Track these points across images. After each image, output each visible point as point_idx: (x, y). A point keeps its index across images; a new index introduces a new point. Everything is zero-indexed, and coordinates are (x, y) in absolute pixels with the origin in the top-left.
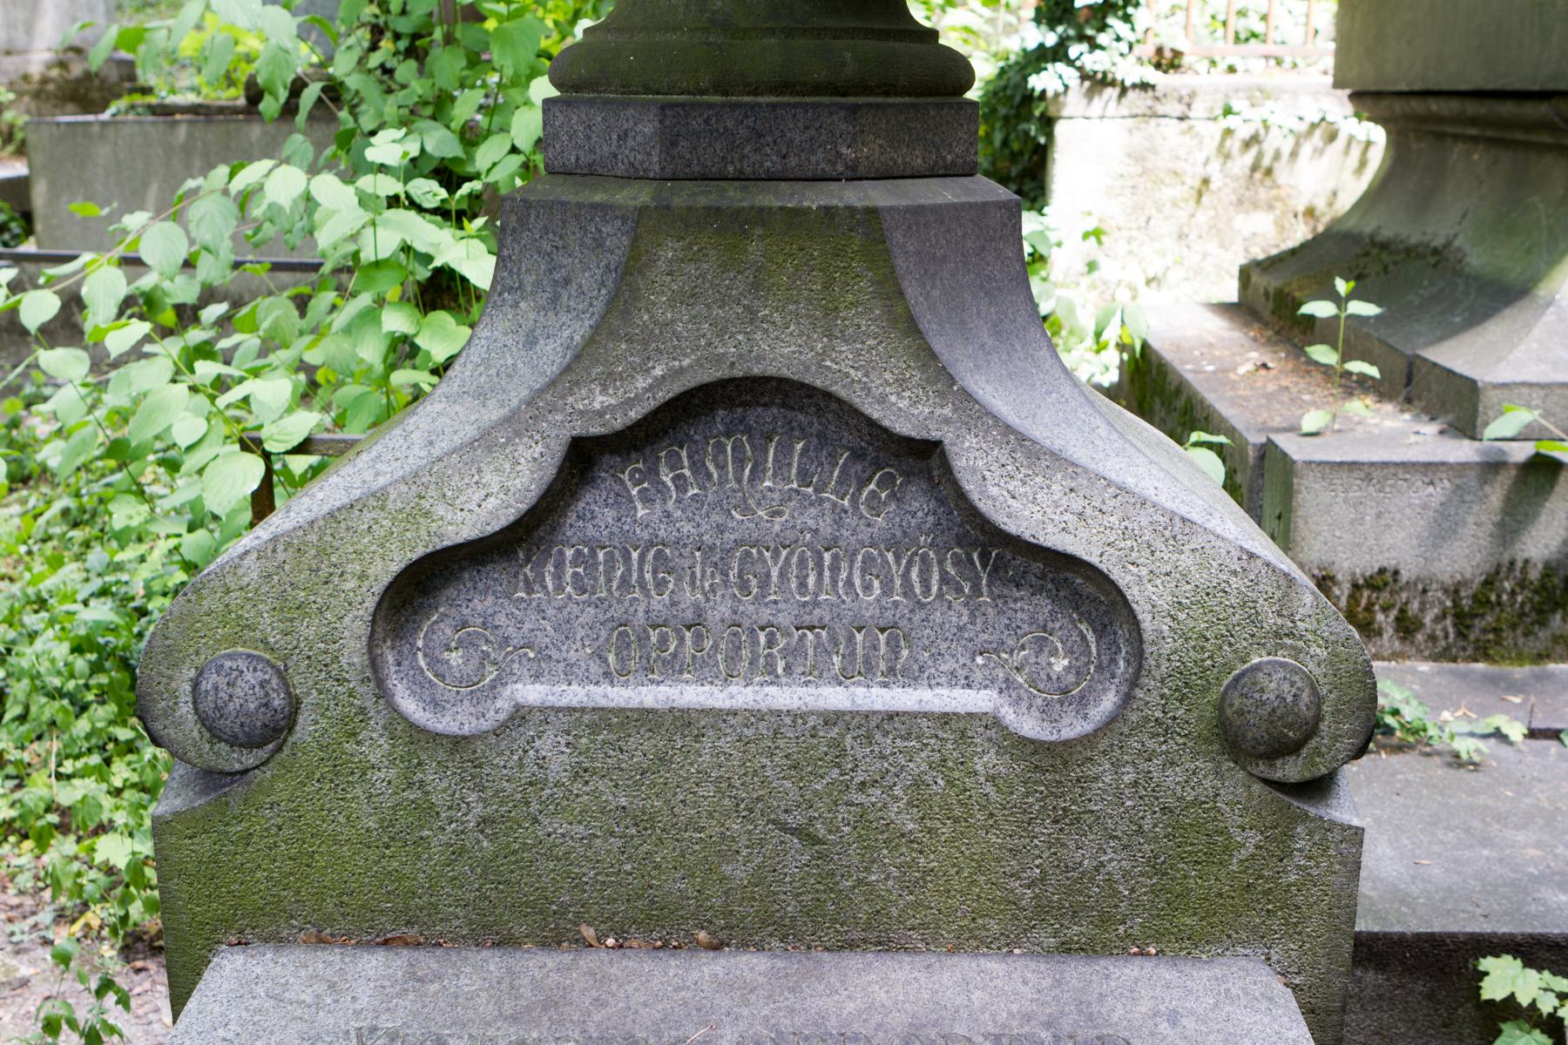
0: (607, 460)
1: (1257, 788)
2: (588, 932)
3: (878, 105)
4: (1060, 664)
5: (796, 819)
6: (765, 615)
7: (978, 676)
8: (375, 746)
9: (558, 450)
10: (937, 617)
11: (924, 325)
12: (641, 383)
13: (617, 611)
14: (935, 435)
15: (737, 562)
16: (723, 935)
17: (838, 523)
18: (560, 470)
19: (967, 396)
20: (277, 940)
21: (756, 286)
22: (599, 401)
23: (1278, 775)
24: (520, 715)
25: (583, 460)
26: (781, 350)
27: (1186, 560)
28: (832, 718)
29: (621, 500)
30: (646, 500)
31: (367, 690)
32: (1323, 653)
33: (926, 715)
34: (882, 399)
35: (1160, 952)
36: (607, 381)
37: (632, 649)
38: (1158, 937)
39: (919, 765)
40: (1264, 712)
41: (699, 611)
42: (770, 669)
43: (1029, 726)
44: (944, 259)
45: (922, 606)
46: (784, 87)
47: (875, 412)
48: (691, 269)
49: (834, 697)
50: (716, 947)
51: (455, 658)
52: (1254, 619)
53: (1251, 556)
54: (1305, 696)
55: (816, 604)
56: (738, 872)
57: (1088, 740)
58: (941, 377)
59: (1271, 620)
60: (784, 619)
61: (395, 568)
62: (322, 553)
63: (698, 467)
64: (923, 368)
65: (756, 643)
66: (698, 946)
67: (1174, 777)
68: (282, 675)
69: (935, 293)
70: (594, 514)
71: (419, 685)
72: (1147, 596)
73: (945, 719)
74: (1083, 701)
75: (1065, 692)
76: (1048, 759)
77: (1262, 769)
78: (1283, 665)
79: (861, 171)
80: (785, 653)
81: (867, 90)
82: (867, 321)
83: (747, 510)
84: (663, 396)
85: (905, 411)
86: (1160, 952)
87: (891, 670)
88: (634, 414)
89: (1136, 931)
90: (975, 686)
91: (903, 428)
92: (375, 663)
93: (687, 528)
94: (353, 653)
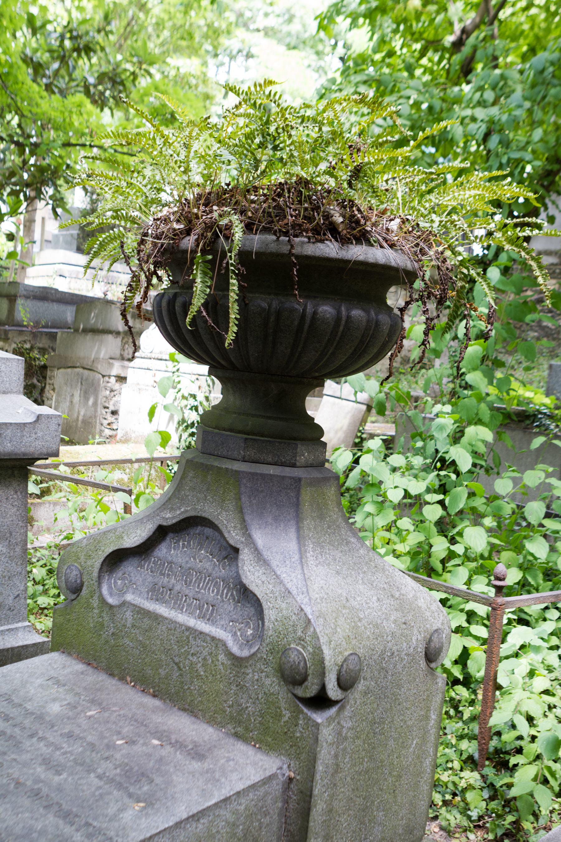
0: (171, 535)
1: (290, 695)
2: (129, 679)
3: (254, 440)
4: (250, 632)
5: (177, 660)
6: (187, 592)
7: (229, 628)
8: (95, 602)
9: (155, 527)
10: (226, 606)
11: (245, 510)
12: (178, 512)
13: (156, 580)
14: (238, 546)
15: (186, 574)
16: (157, 693)
17: (213, 569)
18: (154, 533)
19: (250, 536)
20: (69, 654)
21: (208, 489)
22: (168, 515)
23: (295, 692)
24: (124, 604)
25: (161, 533)
26: (208, 510)
27: (284, 605)
28: (188, 629)
29: (169, 549)
30: (174, 549)
31: (96, 584)
32: (311, 650)
33: (209, 635)
34: (229, 532)
35: (259, 748)
36: (172, 509)
37: (157, 593)
38: (261, 742)
39: (205, 653)
40: (289, 665)
41: (173, 585)
42: (182, 610)
43: (235, 650)
44: (262, 491)
45: (223, 601)
46: (231, 430)
47: (226, 535)
48: (195, 480)
49: (192, 622)
50: (154, 696)
51: (119, 582)
52: (295, 632)
53: (302, 610)
54: (302, 664)
55: (199, 592)
56: (162, 672)
57: (247, 659)
58: (245, 528)
59: (299, 633)
60: (191, 595)
61: (111, 551)
62: (99, 542)
63: (189, 542)
64: (241, 524)
65: (181, 600)
66: (149, 694)
67: (268, 682)
68: (81, 574)
69: (254, 502)
70: (163, 551)
71: (110, 588)
72: (270, 614)
73: (213, 638)
74: (251, 646)
75: (248, 642)
76: (238, 662)
77: (291, 687)
78: (298, 650)
79: (246, 459)
80: (188, 605)
81: (254, 434)
82: (230, 505)
83: (195, 559)
84: (182, 517)
85: (234, 536)
86: (259, 748)
87: (208, 620)
88: (174, 521)
89: (255, 737)
90: (226, 632)
91: (232, 542)
92: (99, 577)
93: (180, 560)
94: (95, 574)
